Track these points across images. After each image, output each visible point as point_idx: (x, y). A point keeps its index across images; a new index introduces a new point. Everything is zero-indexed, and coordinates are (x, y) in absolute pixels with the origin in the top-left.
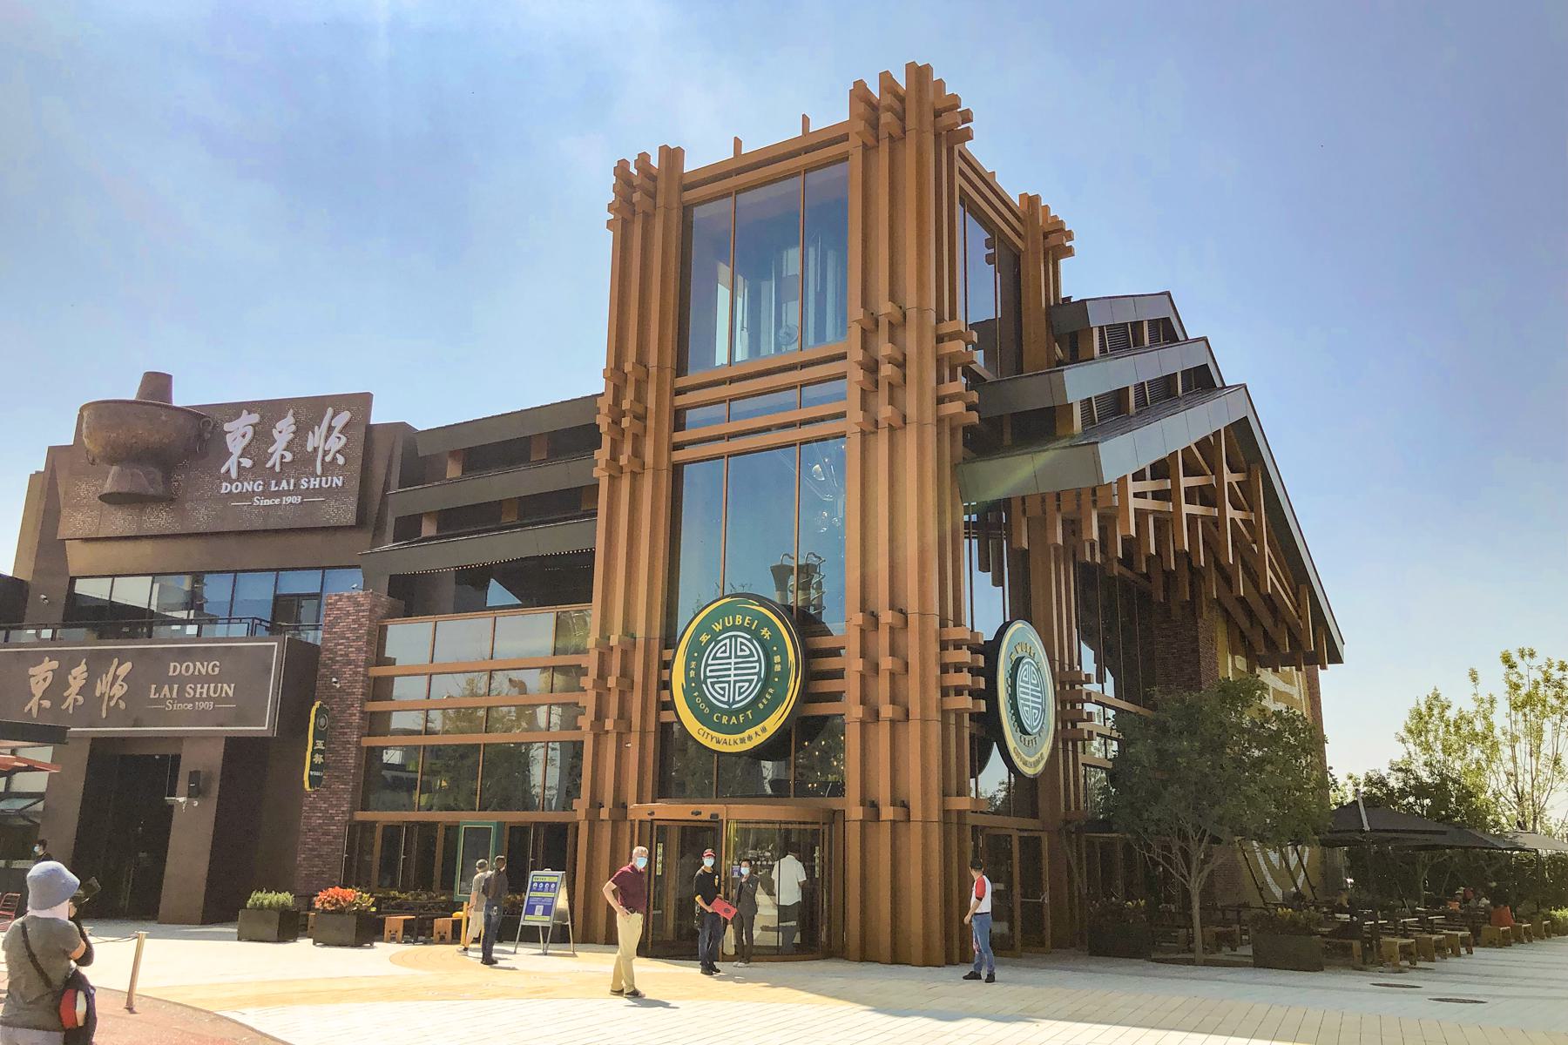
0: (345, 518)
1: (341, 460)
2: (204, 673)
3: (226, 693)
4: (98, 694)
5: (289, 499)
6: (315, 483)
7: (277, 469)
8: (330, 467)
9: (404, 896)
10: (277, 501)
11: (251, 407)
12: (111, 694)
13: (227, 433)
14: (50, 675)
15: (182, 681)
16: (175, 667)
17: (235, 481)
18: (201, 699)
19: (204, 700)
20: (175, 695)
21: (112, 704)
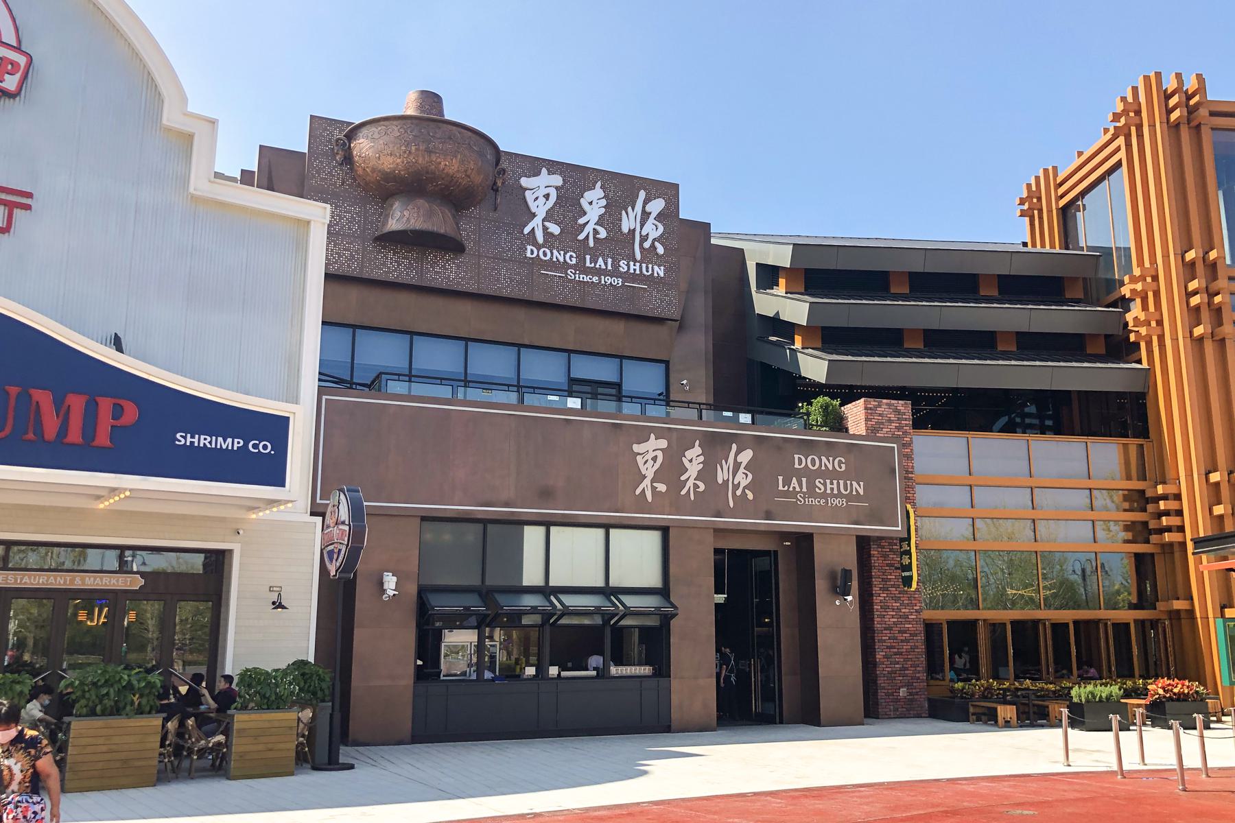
0: (669, 311)
1: (660, 250)
2: (831, 469)
3: (857, 491)
4: (720, 481)
5: (609, 280)
6: (634, 268)
7: (591, 243)
8: (649, 255)
9: (1041, 685)
10: (595, 279)
11: (554, 167)
12: (736, 483)
13: (527, 189)
14: (660, 454)
15: (812, 476)
16: (800, 459)
17: (543, 246)
18: (833, 496)
19: (836, 496)
20: (804, 489)
21: (739, 493)
